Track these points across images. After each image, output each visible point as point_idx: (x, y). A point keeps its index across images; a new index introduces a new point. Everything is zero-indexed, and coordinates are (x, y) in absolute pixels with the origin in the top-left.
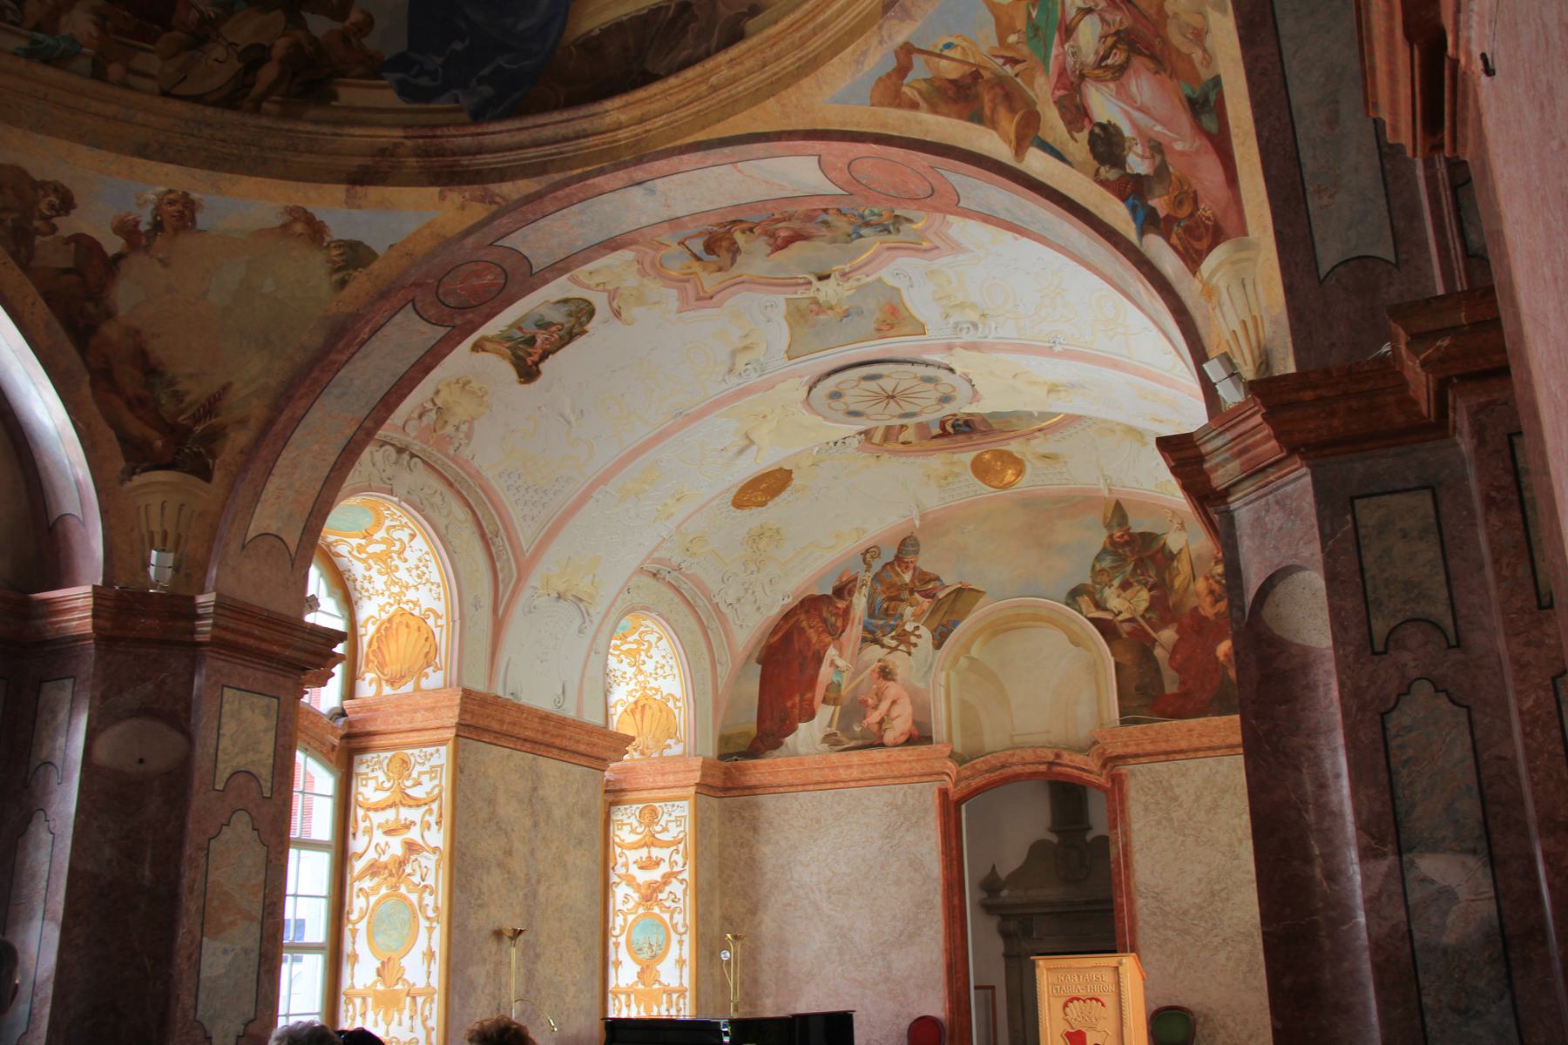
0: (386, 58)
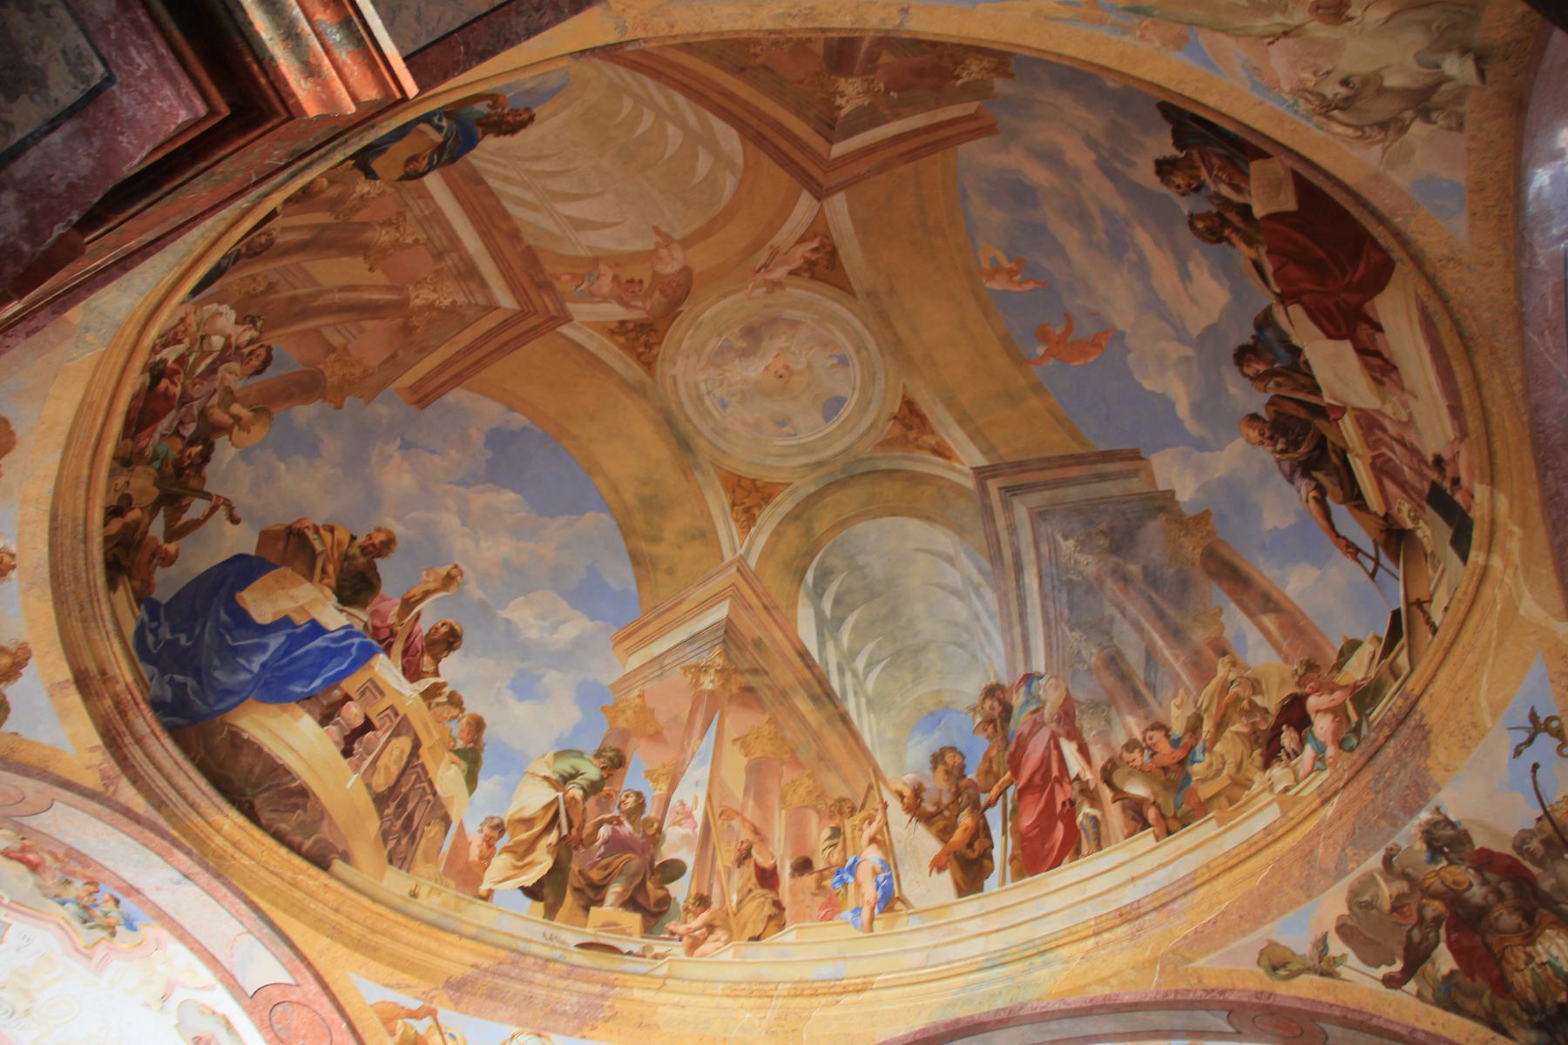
0: (153, 596)
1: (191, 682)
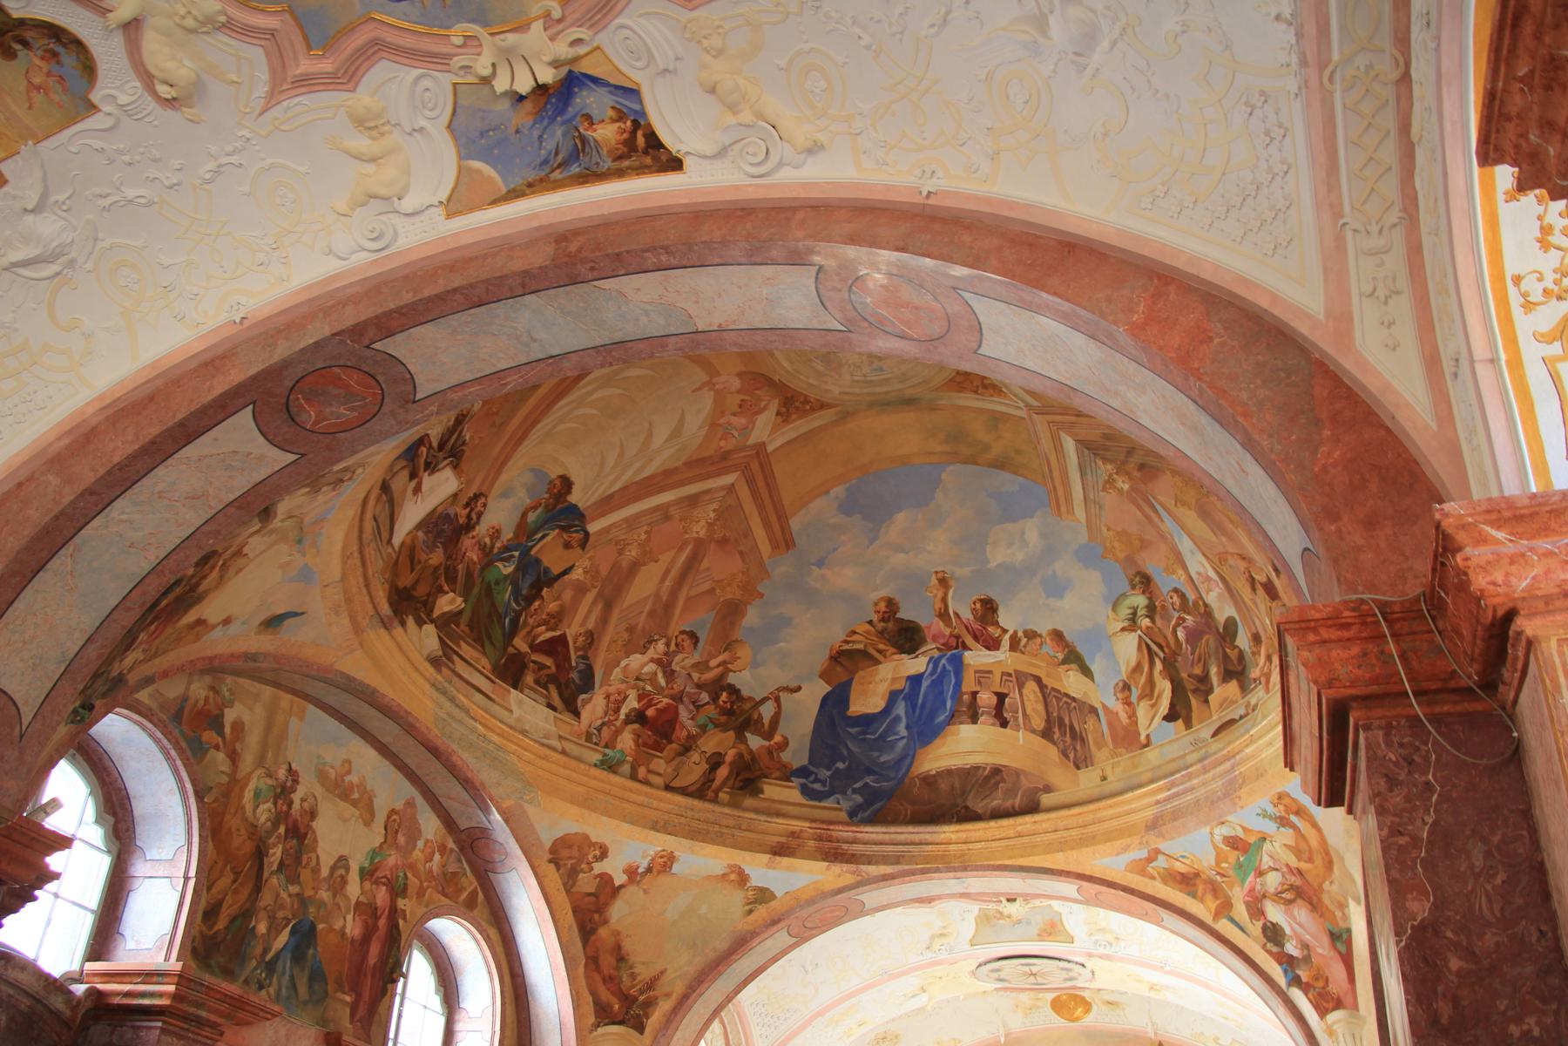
0: (794, 768)
1: (869, 779)
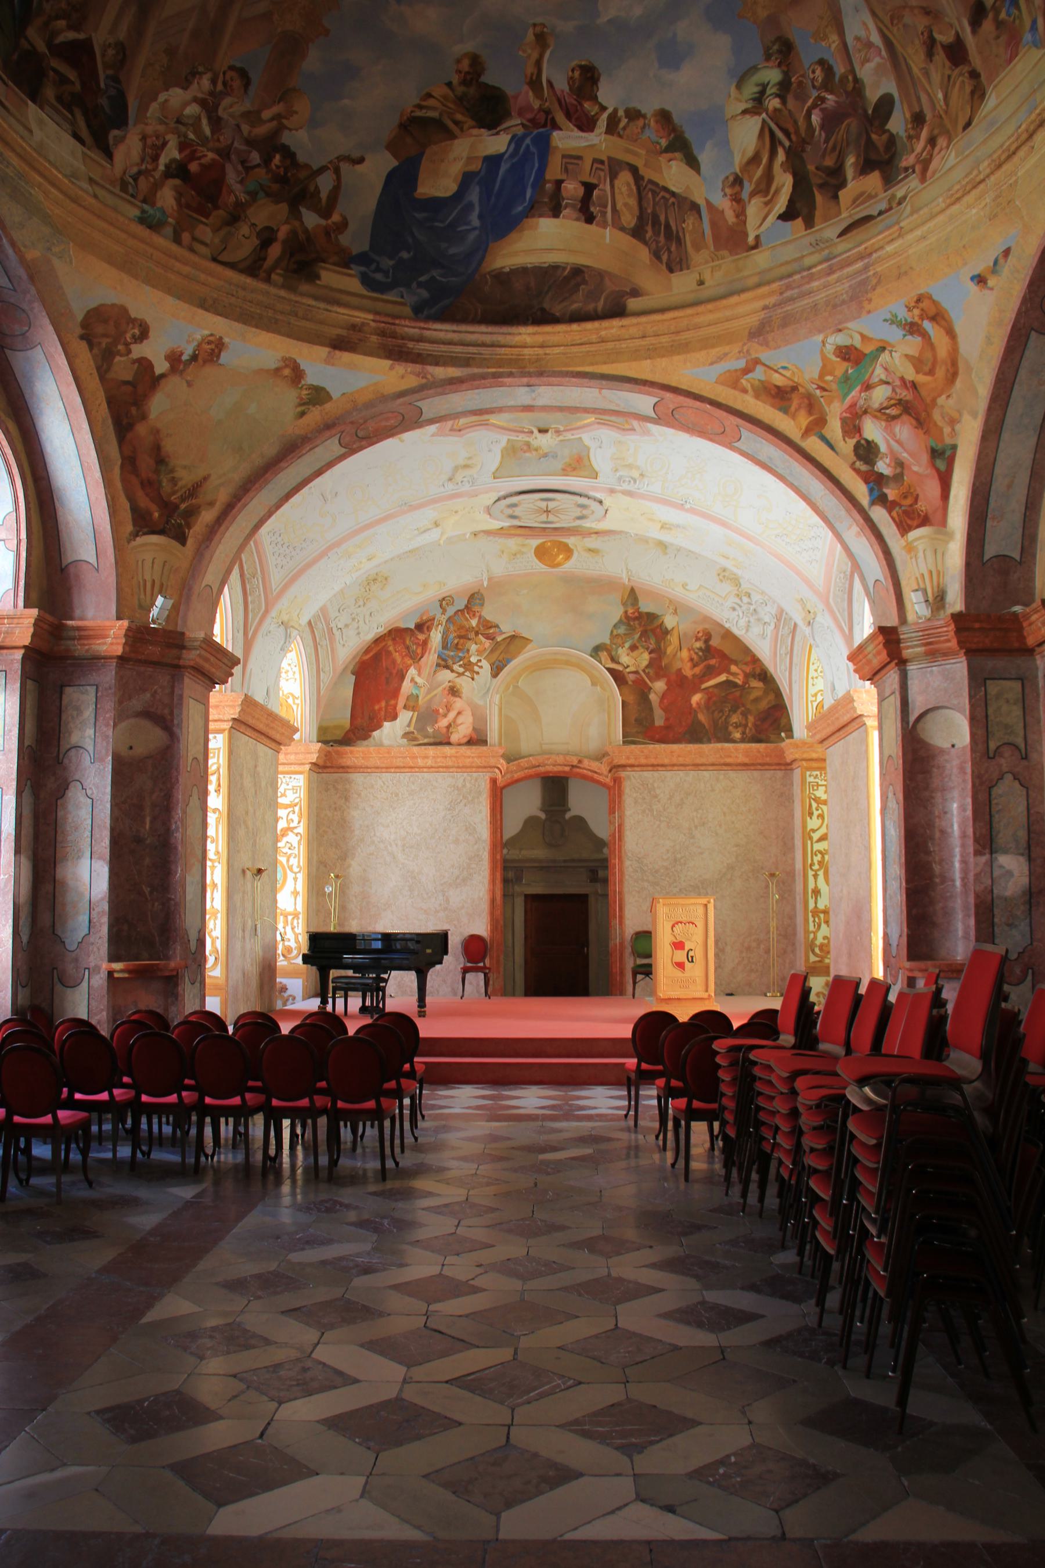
0: (354, 253)
1: (436, 273)
